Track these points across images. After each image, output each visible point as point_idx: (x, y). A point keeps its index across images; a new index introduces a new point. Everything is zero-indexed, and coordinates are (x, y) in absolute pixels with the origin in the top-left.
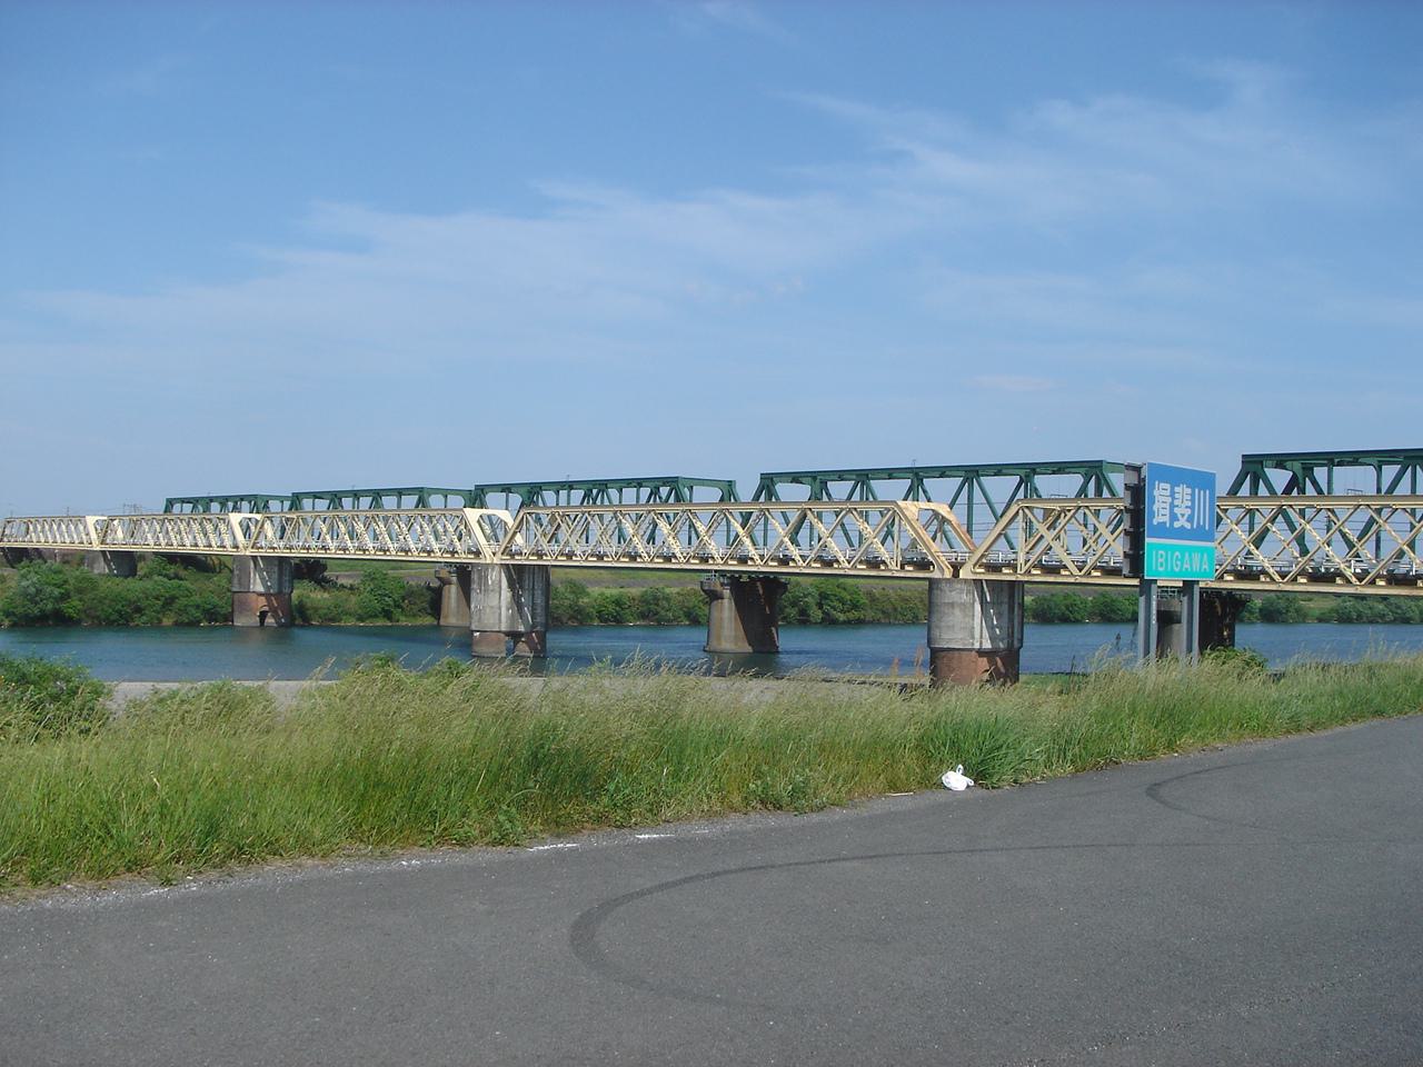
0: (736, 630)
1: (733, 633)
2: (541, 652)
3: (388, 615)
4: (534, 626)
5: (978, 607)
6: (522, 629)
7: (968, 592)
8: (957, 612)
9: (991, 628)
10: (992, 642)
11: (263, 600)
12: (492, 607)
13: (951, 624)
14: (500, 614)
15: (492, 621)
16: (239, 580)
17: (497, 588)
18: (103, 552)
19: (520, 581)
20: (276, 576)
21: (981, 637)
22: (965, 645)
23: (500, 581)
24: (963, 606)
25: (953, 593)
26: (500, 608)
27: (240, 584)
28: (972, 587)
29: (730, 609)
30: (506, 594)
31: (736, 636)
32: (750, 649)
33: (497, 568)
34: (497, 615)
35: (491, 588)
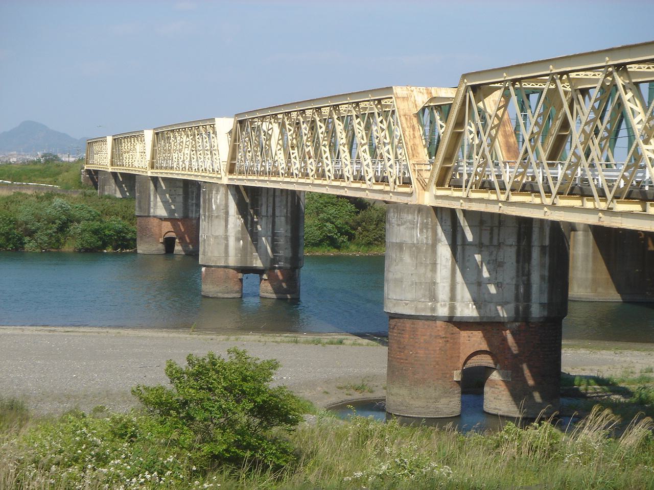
0: (594, 272)
1: (590, 276)
2: (287, 291)
3: (333, 243)
4: (274, 261)
5: (444, 251)
6: (258, 264)
7: (424, 226)
8: (407, 258)
9: (476, 285)
10: (479, 308)
11: (167, 226)
12: (216, 237)
13: (399, 276)
14: (227, 246)
15: (216, 254)
16: (140, 203)
17: (222, 214)
18: (114, 175)
19: (255, 203)
20: (180, 199)
21: (453, 298)
22: (599, 299)
23: (227, 206)
24: (416, 249)
25: (402, 228)
26: (226, 238)
27: (140, 208)
28: (432, 219)
29: (586, 244)
30: (235, 221)
31: (594, 281)
32: (614, 296)
33: (222, 190)
34: (222, 247)
35: (215, 214)
